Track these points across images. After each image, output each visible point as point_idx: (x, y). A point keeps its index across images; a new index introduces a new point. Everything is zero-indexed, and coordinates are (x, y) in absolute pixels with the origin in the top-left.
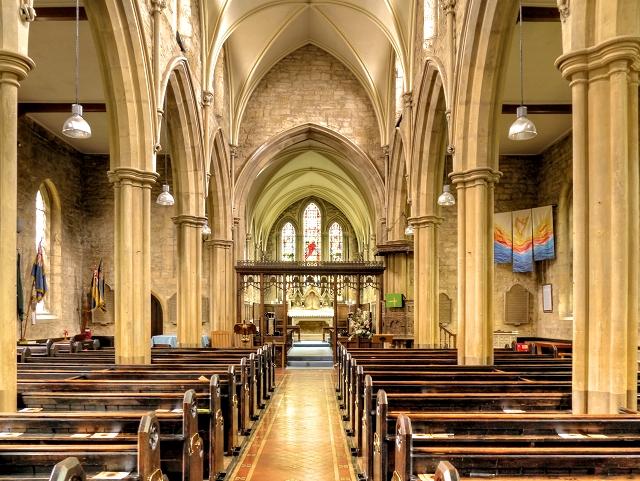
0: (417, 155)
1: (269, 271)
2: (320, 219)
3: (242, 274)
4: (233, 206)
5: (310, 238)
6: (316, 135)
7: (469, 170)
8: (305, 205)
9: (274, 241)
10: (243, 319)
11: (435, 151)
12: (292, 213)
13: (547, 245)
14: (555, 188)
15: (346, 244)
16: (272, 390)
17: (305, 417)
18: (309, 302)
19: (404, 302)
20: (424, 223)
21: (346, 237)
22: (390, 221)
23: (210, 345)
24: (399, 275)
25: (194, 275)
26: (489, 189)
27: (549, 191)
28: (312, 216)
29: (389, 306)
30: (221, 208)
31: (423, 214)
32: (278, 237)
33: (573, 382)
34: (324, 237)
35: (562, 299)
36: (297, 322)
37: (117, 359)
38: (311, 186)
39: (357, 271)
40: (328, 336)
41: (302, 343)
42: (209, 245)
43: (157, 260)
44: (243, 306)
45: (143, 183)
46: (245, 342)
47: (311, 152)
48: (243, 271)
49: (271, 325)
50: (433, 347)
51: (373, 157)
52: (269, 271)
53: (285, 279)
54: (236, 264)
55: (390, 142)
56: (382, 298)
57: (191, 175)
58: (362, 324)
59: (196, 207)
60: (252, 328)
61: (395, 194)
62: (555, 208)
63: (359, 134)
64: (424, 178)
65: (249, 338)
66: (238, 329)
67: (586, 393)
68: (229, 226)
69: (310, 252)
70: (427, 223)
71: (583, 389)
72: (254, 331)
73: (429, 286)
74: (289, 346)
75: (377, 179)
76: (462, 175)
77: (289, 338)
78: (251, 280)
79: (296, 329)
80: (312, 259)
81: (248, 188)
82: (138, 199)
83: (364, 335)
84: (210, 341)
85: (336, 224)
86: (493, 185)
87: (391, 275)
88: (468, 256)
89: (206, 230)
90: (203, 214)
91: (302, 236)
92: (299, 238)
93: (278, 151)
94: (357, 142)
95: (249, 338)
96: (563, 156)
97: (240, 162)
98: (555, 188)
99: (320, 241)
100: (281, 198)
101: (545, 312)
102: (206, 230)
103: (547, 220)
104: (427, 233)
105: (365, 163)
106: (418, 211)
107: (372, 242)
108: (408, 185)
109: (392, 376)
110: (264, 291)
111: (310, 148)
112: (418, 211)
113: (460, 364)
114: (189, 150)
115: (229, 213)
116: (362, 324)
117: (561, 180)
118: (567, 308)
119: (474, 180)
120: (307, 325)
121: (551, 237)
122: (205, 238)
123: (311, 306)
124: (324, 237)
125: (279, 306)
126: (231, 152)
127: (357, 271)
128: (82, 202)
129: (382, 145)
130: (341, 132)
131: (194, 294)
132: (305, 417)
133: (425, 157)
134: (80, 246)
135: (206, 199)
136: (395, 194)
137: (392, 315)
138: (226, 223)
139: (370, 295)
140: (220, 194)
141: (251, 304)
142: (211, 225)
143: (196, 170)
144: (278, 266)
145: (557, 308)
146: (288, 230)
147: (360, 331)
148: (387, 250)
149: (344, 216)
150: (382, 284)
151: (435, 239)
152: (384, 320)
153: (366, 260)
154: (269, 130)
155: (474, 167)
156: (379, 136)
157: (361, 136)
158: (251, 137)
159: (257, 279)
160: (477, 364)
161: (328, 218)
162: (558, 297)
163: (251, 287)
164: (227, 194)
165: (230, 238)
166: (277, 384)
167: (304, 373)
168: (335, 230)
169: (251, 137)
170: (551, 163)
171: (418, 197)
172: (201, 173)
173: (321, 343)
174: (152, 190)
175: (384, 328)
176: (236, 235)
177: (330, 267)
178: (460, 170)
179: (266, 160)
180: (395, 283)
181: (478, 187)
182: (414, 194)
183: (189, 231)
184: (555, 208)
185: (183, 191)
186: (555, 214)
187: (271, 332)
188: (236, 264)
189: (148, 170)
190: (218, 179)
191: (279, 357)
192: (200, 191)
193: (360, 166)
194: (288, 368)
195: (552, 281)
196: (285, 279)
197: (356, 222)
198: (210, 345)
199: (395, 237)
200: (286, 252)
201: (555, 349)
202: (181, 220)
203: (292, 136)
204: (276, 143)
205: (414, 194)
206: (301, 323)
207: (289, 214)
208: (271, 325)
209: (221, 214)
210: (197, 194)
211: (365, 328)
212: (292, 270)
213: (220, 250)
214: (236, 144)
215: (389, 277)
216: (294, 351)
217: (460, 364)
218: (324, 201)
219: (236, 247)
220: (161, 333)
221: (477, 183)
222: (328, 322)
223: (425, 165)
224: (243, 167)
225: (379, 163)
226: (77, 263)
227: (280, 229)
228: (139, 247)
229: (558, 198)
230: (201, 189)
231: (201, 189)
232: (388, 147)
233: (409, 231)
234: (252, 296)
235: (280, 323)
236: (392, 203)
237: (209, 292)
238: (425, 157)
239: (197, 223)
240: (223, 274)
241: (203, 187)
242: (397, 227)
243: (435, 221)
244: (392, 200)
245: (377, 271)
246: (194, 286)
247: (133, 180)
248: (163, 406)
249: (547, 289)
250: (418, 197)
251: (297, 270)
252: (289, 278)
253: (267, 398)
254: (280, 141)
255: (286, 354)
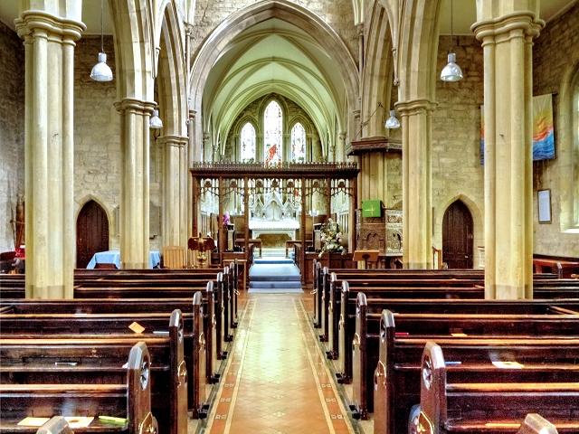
0: (407, 22)
1: (228, 174)
2: (281, 119)
3: (198, 179)
4: (189, 97)
5: (273, 140)
6: (282, 12)
7: (502, 15)
8: (265, 104)
9: (233, 144)
10: (199, 231)
11: (431, 16)
12: (252, 112)
13: (546, 142)
14: (553, 73)
15: (310, 147)
16: (234, 326)
17: (273, 348)
18: (270, 212)
19: (383, 211)
20: (415, 109)
21: (309, 139)
22: (365, 114)
23: (161, 264)
24: (376, 178)
25: (141, 175)
26: (526, 45)
27: (545, 78)
28: (273, 111)
29: (365, 215)
30: (175, 98)
31: (414, 97)
32: (237, 140)
33: (485, 280)
34: (286, 139)
35: (564, 206)
36: (258, 235)
37: (27, 289)
38: (273, 81)
39: (320, 174)
40: (291, 251)
41: (264, 259)
42: (160, 140)
43: (102, 161)
44: (199, 216)
45: (63, 36)
46: (201, 260)
47: (274, 37)
48: (199, 174)
49: (230, 239)
50: (425, 268)
51: (345, 37)
52: (228, 174)
53: (246, 184)
54: (192, 167)
55: (365, 19)
56: (355, 206)
57: (136, 47)
58: (334, 238)
59: (143, 90)
60: (209, 242)
61: (371, 81)
62: (555, 96)
63: (330, 11)
64: (416, 51)
65: (206, 255)
66: (193, 244)
67: (495, 286)
68: (184, 120)
69: (272, 157)
70: (418, 108)
71: (492, 284)
72: (212, 247)
73: (421, 189)
74: (250, 263)
75: (350, 64)
76: (491, 24)
77: (251, 251)
78: (208, 185)
79: (257, 244)
80: (275, 161)
81: (206, 76)
82: (57, 59)
83: (334, 250)
84: (162, 258)
85: (298, 124)
86: (531, 39)
87: (366, 179)
88: (499, 141)
89: (157, 122)
90: (150, 98)
91: (262, 139)
92: (259, 140)
93: (239, 31)
94: (327, 19)
95: (206, 255)
96: (567, 33)
97: (196, 44)
98: (553, 73)
99: (281, 144)
100: (240, 95)
101: (541, 223)
102: (157, 122)
103: (546, 112)
104: (418, 121)
105: (336, 45)
106: (408, 93)
107: (339, 143)
108: (395, 62)
109: (387, 317)
110: (223, 199)
111: (274, 31)
112: (408, 93)
113: (488, 297)
114: (133, 15)
115: (183, 105)
116: (334, 238)
117: (563, 62)
118: (571, 218)
119: (508, 32)
120: (268, 240)
121: (551, 131)
122: (153, 130)
123: (274, 214)
124: (286, 139)
125: (239, 217)
126: (187, 32)
127: (320, 174)
128: (18, 92)
129: (356, 22)
130: (310, 8)
131: (140, 200)
132: (273, 348)
133: (418, 23)
134: (16, 145)
135: (156, 80)
136: (371, 81)
137: (370, 226)
138: (180, 116)
139: (341, 203)
140: (173, 81)
141: (209, 215)
142: (163, 116)
143: (142, 41)
144: (238, 168)
145: (558, 218)
146: (248, 131)
147: (331, 246)
148: (364, 147)
149: (306, 115)
150: (355, 190)
151: (428, 131)
152: (359, 232)
153: (330, 160)
154: (229, 5)
155: (511, 12)
156: (352, 13)
157: (332, 13)
158: (208, 14)
159: (215, 183)
160: (512, 296)
161: (290, 118)
162: (558, 205)
163: (208, 194)
164: (182, 81)
165: (184, 134)
166: (239, 315)
167: (267, 298)
168: (298, 131)
169: (208, 14)
170: (549, 42)
171: (408, 76)
172: (148, 45)
173: (284, 259)
174: (76, 49)
175: (359, 242)
176: (192, 131)
177: (300, 169)
178: (489, 18)
179: (225, 42)
180: (375, 188)
181: (514, 41)
182: (402, 73)
183: (135, 120)
184: (555, 96)
185: (127, 68)
186: (555, 104)
187: (231, 248)
188: (192, 167)
189: (69, 17)
190: (170, 54)
191: (240, 280)
192: (147, 70)
193: (331, 49)
194: (250, 291)
195: (552, 185)
196: (246, 184)
197: (320, 120)
198: (161, 264)
199: (371, 132)
200: (246, 154)
201: (560, 267)
202: (124, 106)
203: (254, 13)
204: (238, 21)
205: (402, 73)
206: (262, 236)
207: (248, 113)
208: (230, 239)
209: (175, 105)
210: (144, 72)
211: (337, 242)
212: (255, 172)
213: (174, 149)
214: (192, 21)
215: (364, 181)
216: (256, 270)
217: (488, 297)
218: (286, 99)
219: (192, 145)
220: (107, 249)
221: (513, 35)
222: (290, 235)
223: (417, 34)
224: (199, 49)
225: (352, 44)
226: (12, 166)
227: (240, 128)
228: (57, 126)
229: (559, 84)
230: (149, 67)
231: (149, 67)
232: (363, 25)
233: (391, 123)
234: (209, 205)
235: (239, 236)
236: (367, 91)
237: (161, 201)
238: (418, 23)
239: (144, 109)
240: (179, 180)
241: (151, 64)
242: (373, 120)
243: (428, 106)
244: (367, 87)
245: (351, 174)
246: (141, 190)
247: (137, 109)
248: (37, 410)
249: (544, 195)
250: (408, 76)
251: (258, 173)
252: (251, 183)
253: (229, 339)
254: (242, 18)
255: (248, 274)
